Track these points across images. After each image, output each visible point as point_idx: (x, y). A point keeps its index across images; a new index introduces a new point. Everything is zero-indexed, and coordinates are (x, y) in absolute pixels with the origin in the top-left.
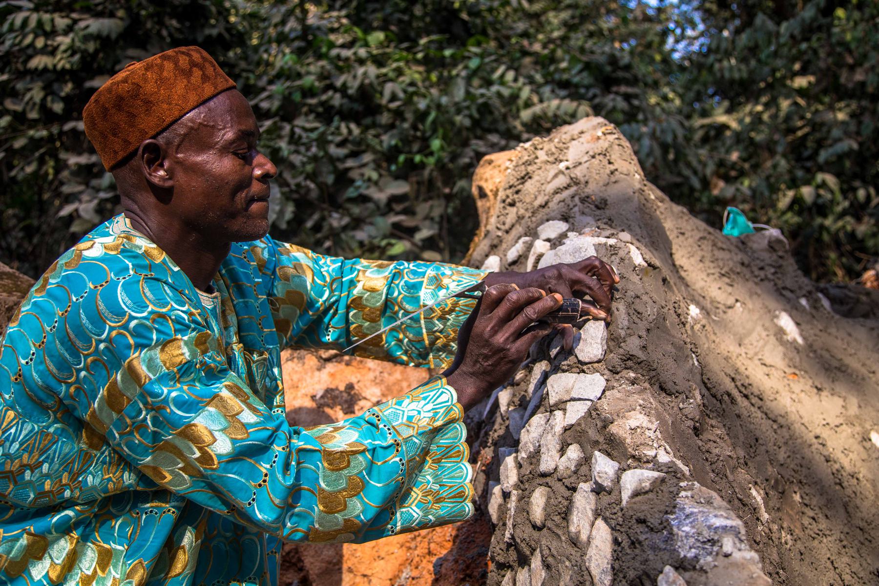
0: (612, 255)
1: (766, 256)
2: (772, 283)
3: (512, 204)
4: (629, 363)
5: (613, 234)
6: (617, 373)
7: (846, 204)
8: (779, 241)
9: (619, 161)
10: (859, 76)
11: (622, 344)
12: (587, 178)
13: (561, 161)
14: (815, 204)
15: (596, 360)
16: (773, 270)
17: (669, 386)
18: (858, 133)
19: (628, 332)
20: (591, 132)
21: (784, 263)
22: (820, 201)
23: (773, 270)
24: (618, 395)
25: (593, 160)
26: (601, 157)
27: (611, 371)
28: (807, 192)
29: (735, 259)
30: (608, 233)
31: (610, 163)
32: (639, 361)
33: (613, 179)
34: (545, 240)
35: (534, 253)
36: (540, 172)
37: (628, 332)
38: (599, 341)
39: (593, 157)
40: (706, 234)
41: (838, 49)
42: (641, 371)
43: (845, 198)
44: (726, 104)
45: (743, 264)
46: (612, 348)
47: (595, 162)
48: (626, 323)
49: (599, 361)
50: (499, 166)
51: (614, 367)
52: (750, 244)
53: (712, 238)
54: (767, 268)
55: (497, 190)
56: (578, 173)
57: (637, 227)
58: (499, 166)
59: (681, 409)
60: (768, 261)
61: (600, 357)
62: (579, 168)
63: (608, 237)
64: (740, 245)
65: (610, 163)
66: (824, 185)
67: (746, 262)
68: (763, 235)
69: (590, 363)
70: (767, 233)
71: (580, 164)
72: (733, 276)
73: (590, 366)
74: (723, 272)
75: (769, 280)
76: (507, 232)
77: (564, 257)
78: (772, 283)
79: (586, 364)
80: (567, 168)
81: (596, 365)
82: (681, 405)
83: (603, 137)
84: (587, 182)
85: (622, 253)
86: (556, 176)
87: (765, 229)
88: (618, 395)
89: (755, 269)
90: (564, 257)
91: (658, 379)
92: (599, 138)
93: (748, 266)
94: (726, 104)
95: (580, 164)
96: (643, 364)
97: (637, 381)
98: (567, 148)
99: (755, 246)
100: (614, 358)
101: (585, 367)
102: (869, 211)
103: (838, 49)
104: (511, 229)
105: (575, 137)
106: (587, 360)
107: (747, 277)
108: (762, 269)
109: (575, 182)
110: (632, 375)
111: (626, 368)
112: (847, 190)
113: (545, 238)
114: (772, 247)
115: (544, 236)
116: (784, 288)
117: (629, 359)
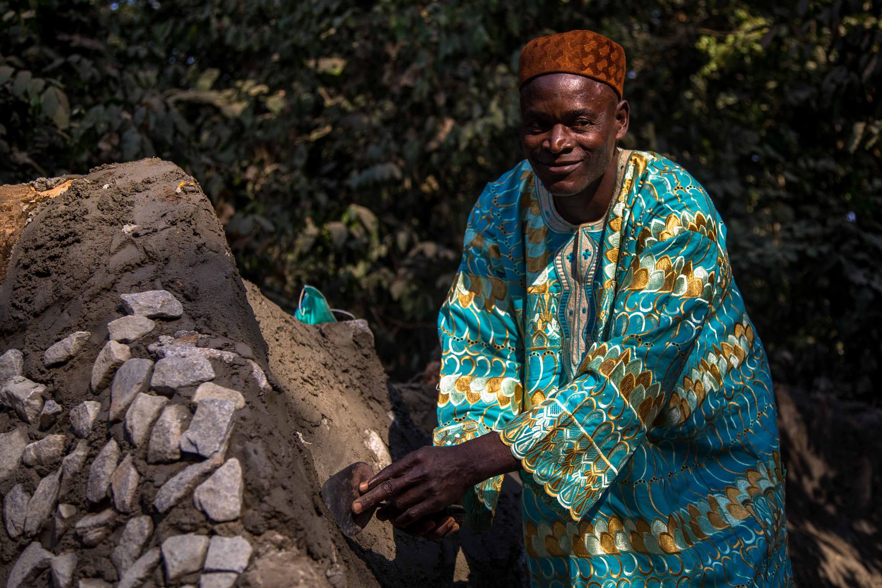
0: (233, 374)
1: (348, 353)
2: (358, 390)
3: (44, 274)
4: (274, 522)
5: (227, 345)
6: (259, 534)
7: (383, 250)
8: (365, 335)
9: (207, 232)
10: (406, 80)
11: (266, 498)
12: (166, 254)
13: (125, 222)
14: (346, 247)
15: (232, 517)
16: (358, 374)
17: (316, 549)
18: (400, 155)
19: (273, 482)
20: (163, 184)
21: (370, 364)
22: (352, 245)
23: (358, 374)
24: (272, 565)
25: (174, 228)
26: (183, 225)
27: (251, 532)
28: (336, 228)
29: (317, 359)
30: (220, 342)
31: (195, 234)
32: (286, 518)
33: (201, 257)
34: (121, 342)
35: (106, 360)
36: (93, 234)
37: (273, 482)
38: (236, 493)
39: (173, 224)
40: (283, 324)
41: (381, 36)
42: (286, 531)
43: (381, 241)
44: (215, 73)
45: (325, 365)
46: (248, 501)
47: (177, 230)
48: (269, 470)
49: (235, 520)
50: (10, 209)
51: (255, 527)
52: (331, 337)
53: (290, 328)
54: (352, 370)
55: (9, 247)
56: (153, 243)
57: (235, 327)
58: (10, 209)
59: (328, 577)
60: (352, 361)
61: (238, 514)
62: (155, 237)
63: (220, 349)
64: (320, 337)
65: (195, 234)
66: (359, 220)
67: (330, 363)
68: (348, 325)
69: (224, 522)
70: (352, 323)
71: (155, 231)
72: (317, 383)
73: (223, 525)
74: (305, 376)
75: (355, 387)
76: (36, 315)
77: (170, 374)
78: (358, 390)
79: (218, 522)
80: (136, 235)
81: (231, 525)
82: (329, 573)
83: (184, 196)
84: (167, 259)
85: (243, 372)
86: (122, 245)
87: (351, 319)
88: (272, 565)
89: (338, 372)
90: (170, 374)
91: (306, 542)
92: (177, 196)
93: (331, 368)
94: (215, 73)
95: (155, 231)
96: (289, 523)
97: (284, 545)
98: (131, 204)
99: (338, 340)
100: (256, 516)
101: (216, 527)
102: (408, 261)
103: (381, 36)
104: (43, 312)
105: (141, 188)
106: (221, 518)
107: (332, 383)
108: (346, 371)
109: (150, 257)
110: (279, 537)
111: (270, 528)
112: (386, 231)
113: (120, 338)
114: (356, 343)
115: (117, 334)
116: (371, 398)
117: (274, 517)
